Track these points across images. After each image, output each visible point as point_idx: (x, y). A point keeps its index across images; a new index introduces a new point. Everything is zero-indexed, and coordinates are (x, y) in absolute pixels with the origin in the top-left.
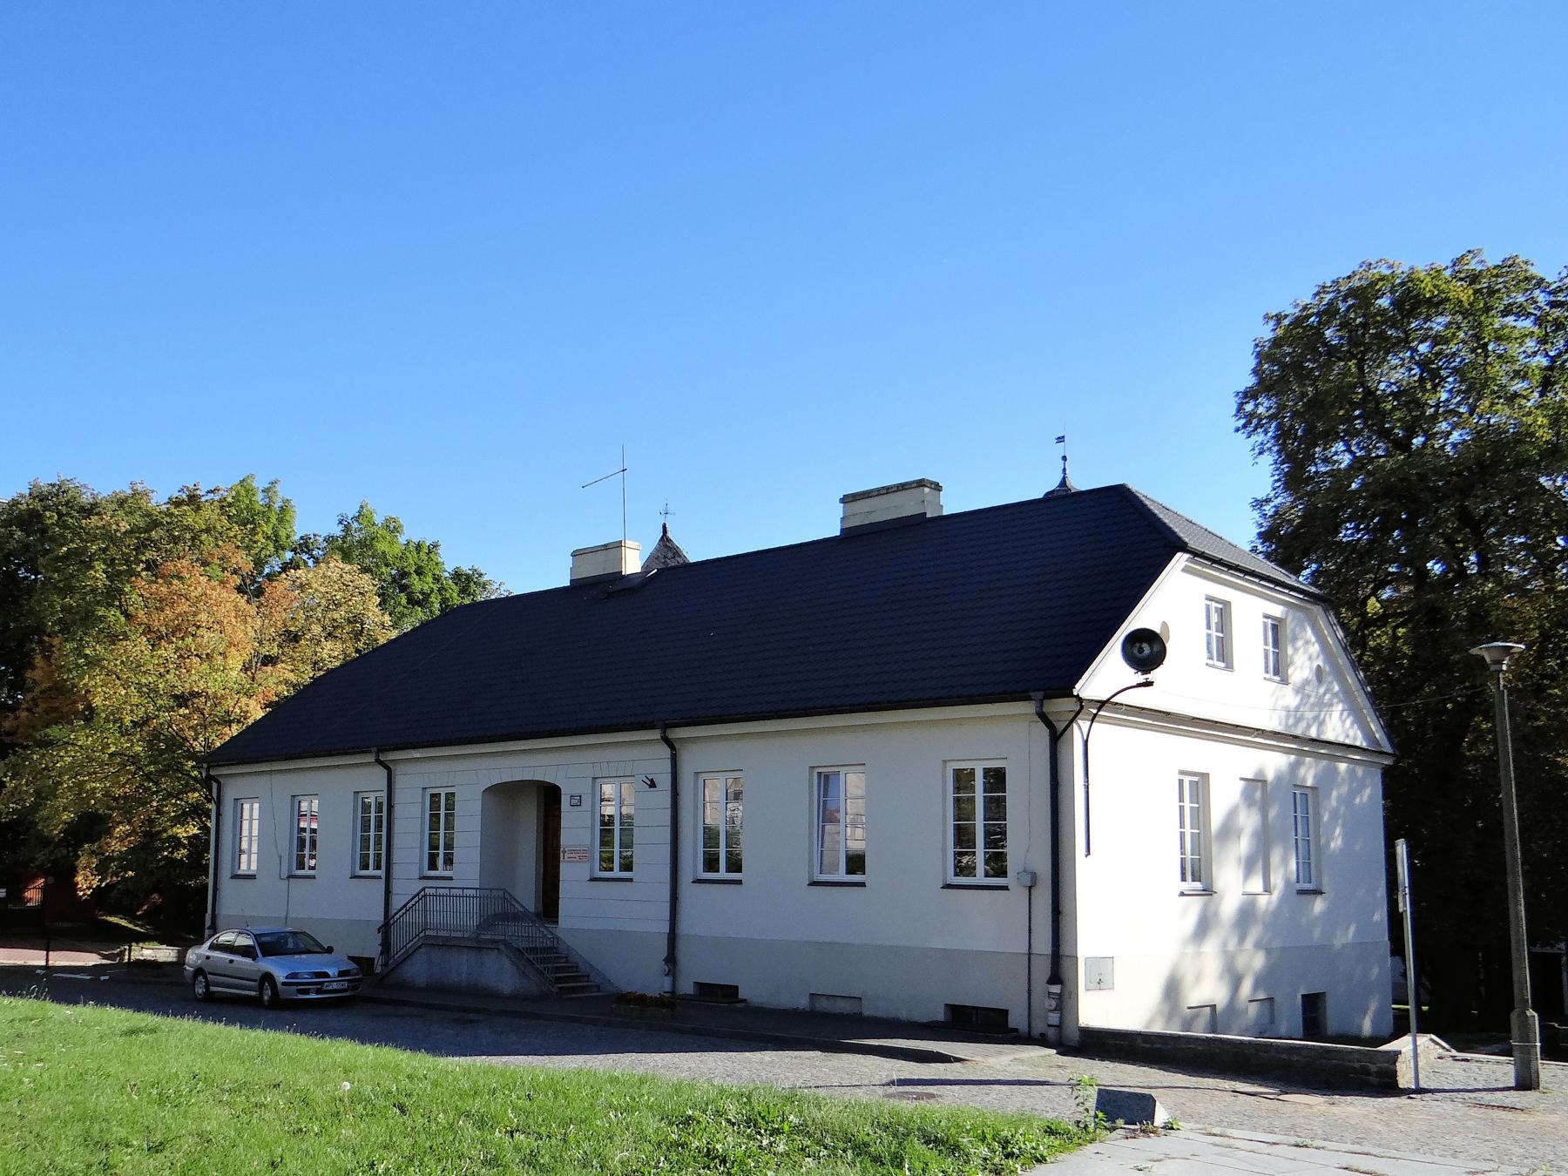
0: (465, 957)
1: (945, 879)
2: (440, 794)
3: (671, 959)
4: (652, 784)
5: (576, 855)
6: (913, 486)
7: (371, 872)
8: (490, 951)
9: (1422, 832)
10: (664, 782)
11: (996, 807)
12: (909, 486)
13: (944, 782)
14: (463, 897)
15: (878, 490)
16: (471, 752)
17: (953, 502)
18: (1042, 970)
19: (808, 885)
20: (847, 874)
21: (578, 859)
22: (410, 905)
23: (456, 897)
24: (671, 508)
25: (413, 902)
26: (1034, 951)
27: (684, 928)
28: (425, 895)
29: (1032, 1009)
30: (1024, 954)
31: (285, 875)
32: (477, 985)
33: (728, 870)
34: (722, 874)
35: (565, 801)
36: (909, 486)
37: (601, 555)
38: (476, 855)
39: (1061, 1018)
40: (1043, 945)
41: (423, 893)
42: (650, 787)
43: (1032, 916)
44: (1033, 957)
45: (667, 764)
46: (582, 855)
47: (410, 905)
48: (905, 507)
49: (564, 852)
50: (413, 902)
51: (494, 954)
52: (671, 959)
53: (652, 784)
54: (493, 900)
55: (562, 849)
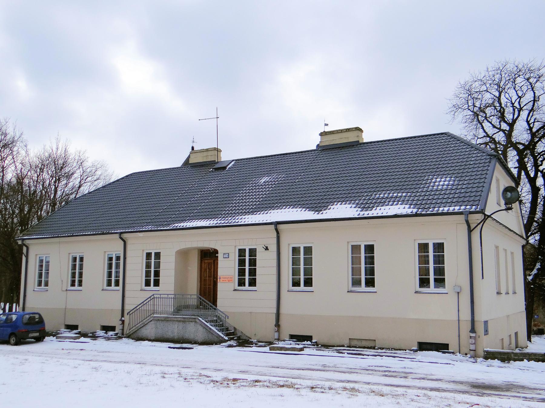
0: (176, 326)
1: (348, 290)
2: (360, 246)
3: (278, 325)
4: (267, 249)
5: (227, 280)
6: (353, 129)
7: (113, 287)
8: (190, 323)
9: (541, 273)
10: (273, 248)
11: (440, 260)
12: (352, 130)
13: (69, 261)
14: (160, 298)
15: (337, 131)
16: (45, 242)
17: (366, 138)
18: (466, 327)
19: (233, 290)
20: (292, 286)
21: (227, 281)
22: (145, 302)
23: (158, 298)
24: (195, 140)
25: (147, 301)
26: (461, 319)
27: (283, 311)
28: (154, 298)
29: (461, 343)
30: (470, 321)
31: (64, 289)
32: (183, 337)
33: (305, 286)
34: (43, 286)
35: (220, 256)
36: (352, 130)
37: (205, 154)
38: (172, 280)
39: (476, 347)
40: (466, 315)
41: (153, 297)
42: (266, 250)
43: (459, 305)
44: (460, 321)
45: (275, 241)
46: (229, 280)
47: (145, 302)
48: (351, 138)
49: (220, 278)
50: (147, 301)
51: (192, 324)
52: (278, 325)
53: (267, 249)
54: (180, 299)
55: (218, 277)
